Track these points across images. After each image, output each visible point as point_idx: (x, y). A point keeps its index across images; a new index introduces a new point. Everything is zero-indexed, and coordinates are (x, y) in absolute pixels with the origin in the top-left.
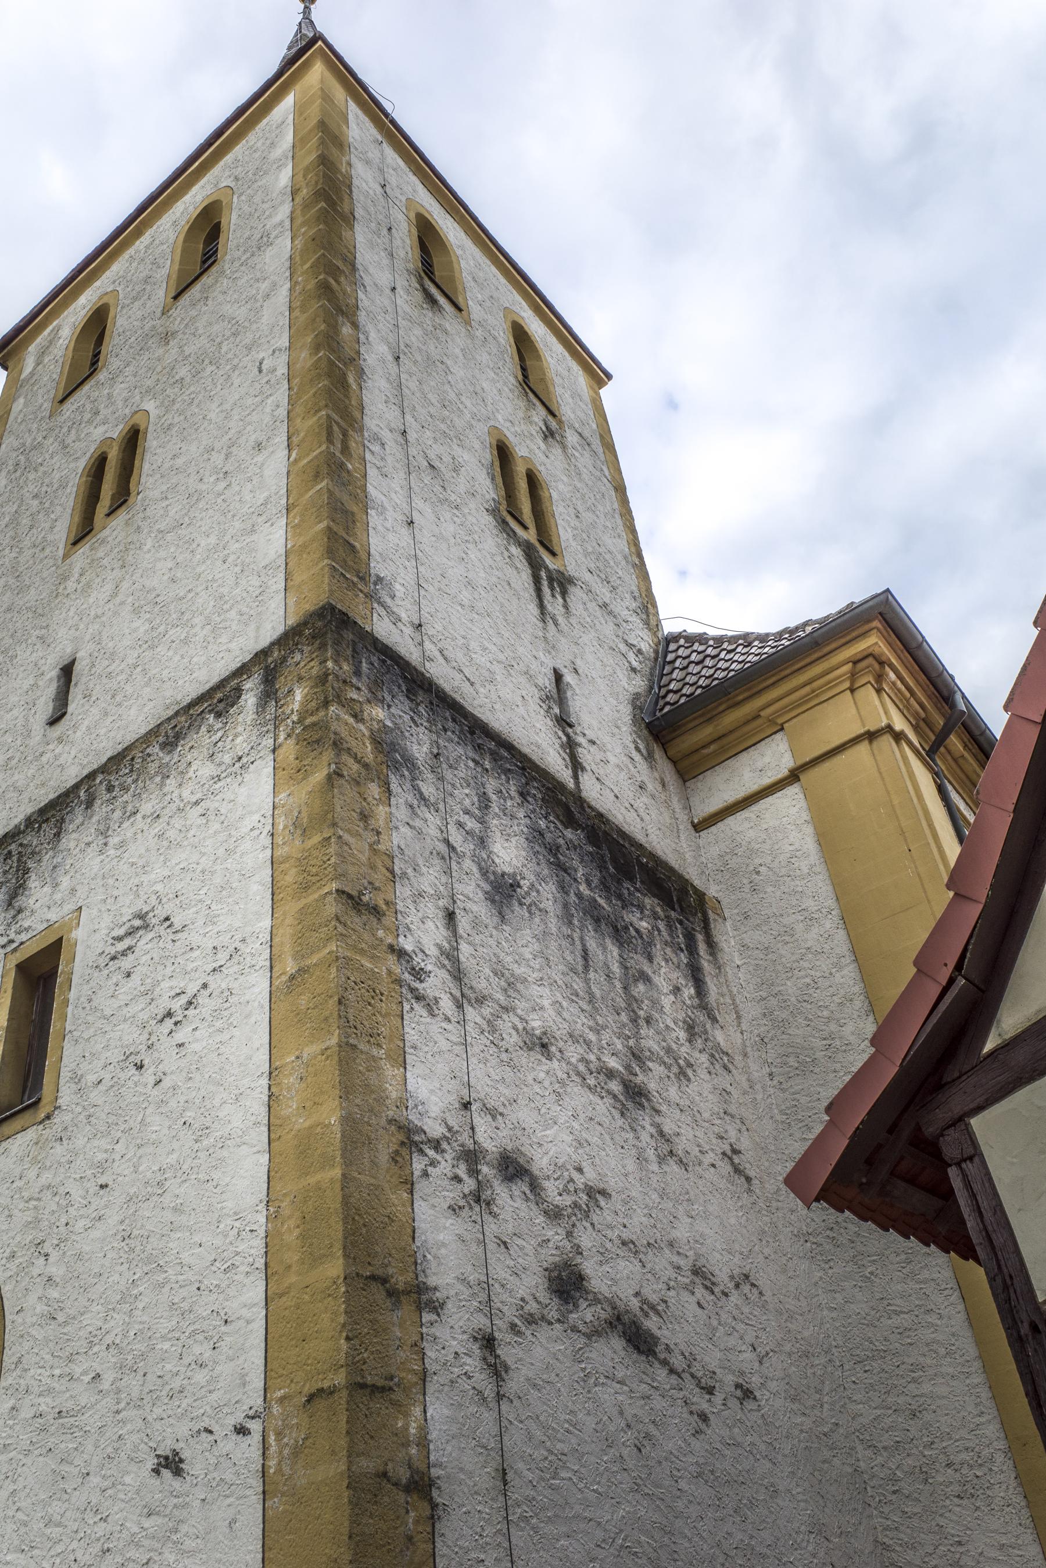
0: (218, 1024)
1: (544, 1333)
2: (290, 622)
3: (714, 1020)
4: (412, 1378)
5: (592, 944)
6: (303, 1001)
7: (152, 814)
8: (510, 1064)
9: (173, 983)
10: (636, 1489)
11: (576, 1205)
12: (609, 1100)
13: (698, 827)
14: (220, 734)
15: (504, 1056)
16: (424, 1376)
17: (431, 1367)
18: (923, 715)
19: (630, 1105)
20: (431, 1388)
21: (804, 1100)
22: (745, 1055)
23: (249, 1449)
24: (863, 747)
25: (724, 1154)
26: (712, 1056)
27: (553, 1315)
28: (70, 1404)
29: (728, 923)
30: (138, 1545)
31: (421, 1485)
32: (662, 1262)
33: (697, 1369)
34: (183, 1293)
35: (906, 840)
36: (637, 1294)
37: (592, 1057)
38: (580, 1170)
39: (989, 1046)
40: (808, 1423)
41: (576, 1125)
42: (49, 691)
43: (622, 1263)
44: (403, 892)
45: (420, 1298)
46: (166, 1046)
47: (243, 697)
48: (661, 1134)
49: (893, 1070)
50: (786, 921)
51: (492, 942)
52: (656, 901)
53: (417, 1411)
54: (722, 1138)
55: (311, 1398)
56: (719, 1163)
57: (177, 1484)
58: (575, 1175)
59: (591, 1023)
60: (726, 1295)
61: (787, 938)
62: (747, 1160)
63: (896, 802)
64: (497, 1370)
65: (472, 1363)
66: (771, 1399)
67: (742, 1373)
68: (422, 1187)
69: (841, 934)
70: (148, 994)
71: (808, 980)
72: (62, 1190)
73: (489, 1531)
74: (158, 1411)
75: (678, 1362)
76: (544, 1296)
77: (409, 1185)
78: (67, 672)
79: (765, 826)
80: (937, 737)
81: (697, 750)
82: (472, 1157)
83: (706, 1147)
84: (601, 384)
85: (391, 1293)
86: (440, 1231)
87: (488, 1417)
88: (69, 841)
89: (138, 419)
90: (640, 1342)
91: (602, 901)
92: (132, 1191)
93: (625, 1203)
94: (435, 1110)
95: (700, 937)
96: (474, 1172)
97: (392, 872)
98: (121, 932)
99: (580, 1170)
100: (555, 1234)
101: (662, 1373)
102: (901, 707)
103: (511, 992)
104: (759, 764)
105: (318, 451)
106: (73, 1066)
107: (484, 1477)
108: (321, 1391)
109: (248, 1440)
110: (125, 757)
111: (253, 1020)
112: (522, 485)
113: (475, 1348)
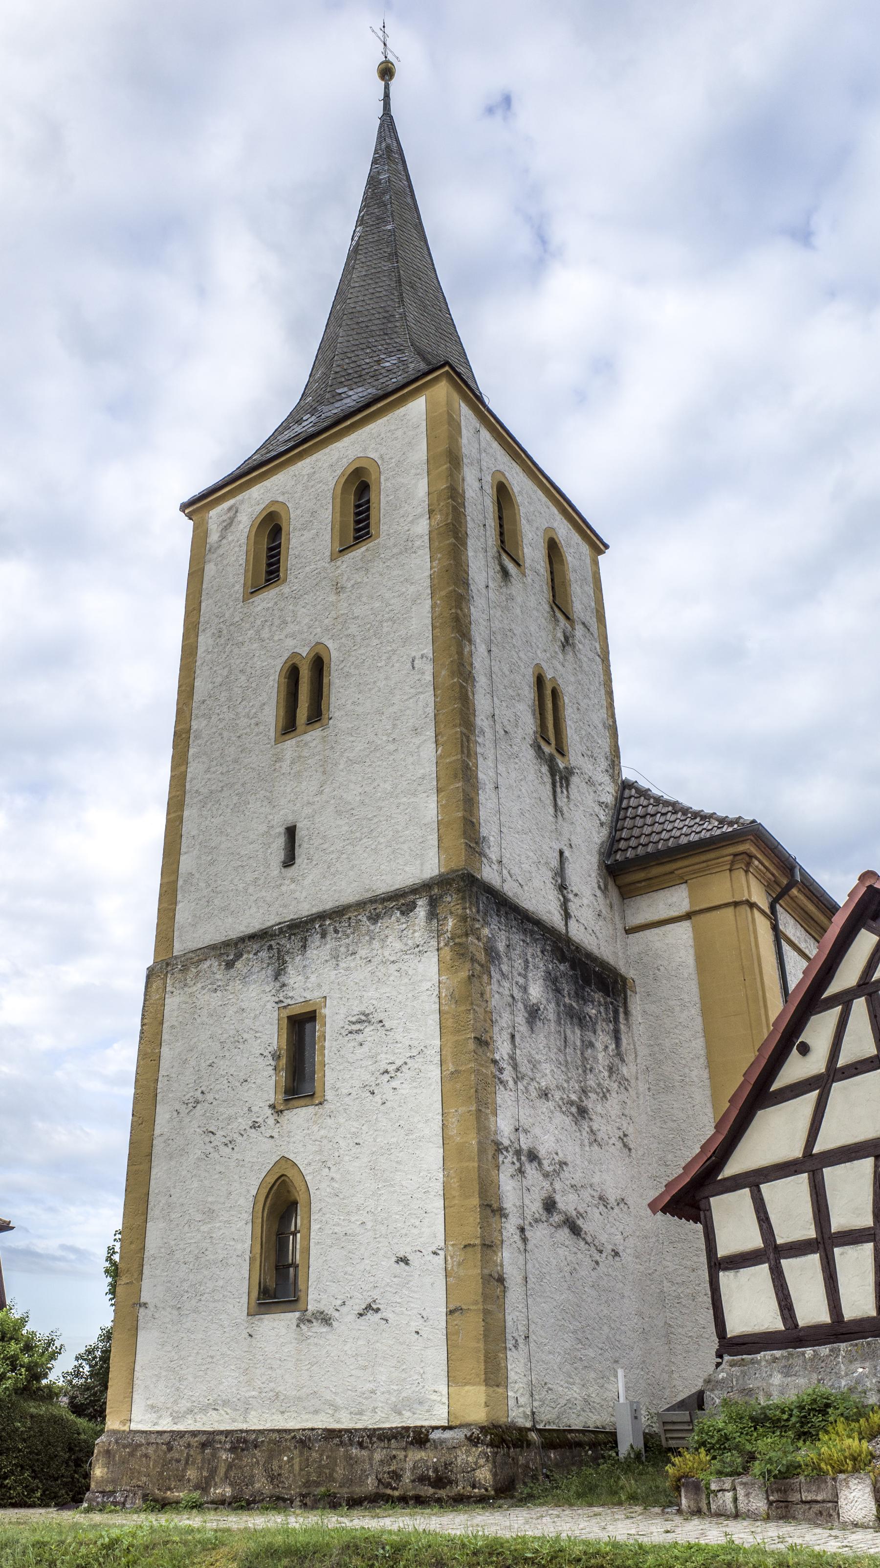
0: (414, 1084)
1: (541, 1226)
2: (442, 870)
3: (623, 1060)
4: (499, 1243)
5: (568, 1032)
6: (458, 1086)
7: (366, 958)
8: (533, 1107)
9: (388, 1056)
10: (569, 1288)
11: (555, 1170)
12: (571, 1117)
13: (629, 931)
14: (404, 926)
15: (531, 1103)
16: (502, 1242)
17: (505, 1239)
18: (773, 879)
19: (579, 1118)
20: (504, 1246)
21: (665, 1106)
22: (637, 1079)
23: (439, 1260)
24: (730, 911)
25: (620, 1137)
26: (620, 1083)
27: (544, 1219)
28: (350, 1232)
29: (638, 996)
30: (391, 1286)
31: (501, 1280)
32: (586, 1194)
33: (596, 1242)
34: (404, 1197)
35: (744, 973)
36: (575, 1209)
37: (565, 1096)
38: (557, 1154)
39: (719, 1178)
40: (642, 1268)
41: (556, 1132)
42: (280, 842)
43: (571, 1196)
44: (496, 1029)
45: (500, 1212)
46: (386, 1088)
47: (417, 909)
48: (592, 1131)
49: (688, 1180)
50: (671, 1003)
51: (528, 1045)
52: (601, 994)
53: (500, 1254)
54: (619, 1129)
55: (465, 1246)
56: (616, 1143)
57: (407, 1268)
58: (555, 1156)
59: (566, 1078)
60: (612, 1208)
61: (670, 1014)
62: (631, 1141)
63: (742, 948)
64: (525, 1240)
65: (517, 1238)
66: (627, 1257)
67: (615, 1245)
68: (502, 1168)
69: (699, 1020)
70: (374, 1058)
71: (677, 1041)
72: (335, 1141)
73: (520, 1297)
74: (396, 1241)
75: (589, 1239)
76: (541, 1211)
77: (498, 1167)
78: (291, 832)
79: (667, 942)
80: (782, 889)
81: (634, 883)
82: (518, 1153)
83: (611, 1135)
84: (601, 552)
85: (493, 1211)
86: (508, 1188)
87: (522, 1258)
88: (312, 953)
89: (319, 649)
90: (575, 1230)
91: (574, 1004)
92: (374, 1149)
93: (574, 1167)
94: (506, 1134)
95: (621, 1010)
96: (519, 1160)
97: (492, 1021)
98: (354, 1019)
99: (557, 1154)
100: (546, 1184)
101: (582, 1243)
102: (759, 877)
103: (535, 1071)
104: (670, 901)
105: (454, 758)
106: (332, 1082)
107: (519, 1279)
108: (470, 1245)
109: (438, 1257)
110: (343, 915)
111: (432, 1087)
112: (548, 692)
113: (518, 1232)
